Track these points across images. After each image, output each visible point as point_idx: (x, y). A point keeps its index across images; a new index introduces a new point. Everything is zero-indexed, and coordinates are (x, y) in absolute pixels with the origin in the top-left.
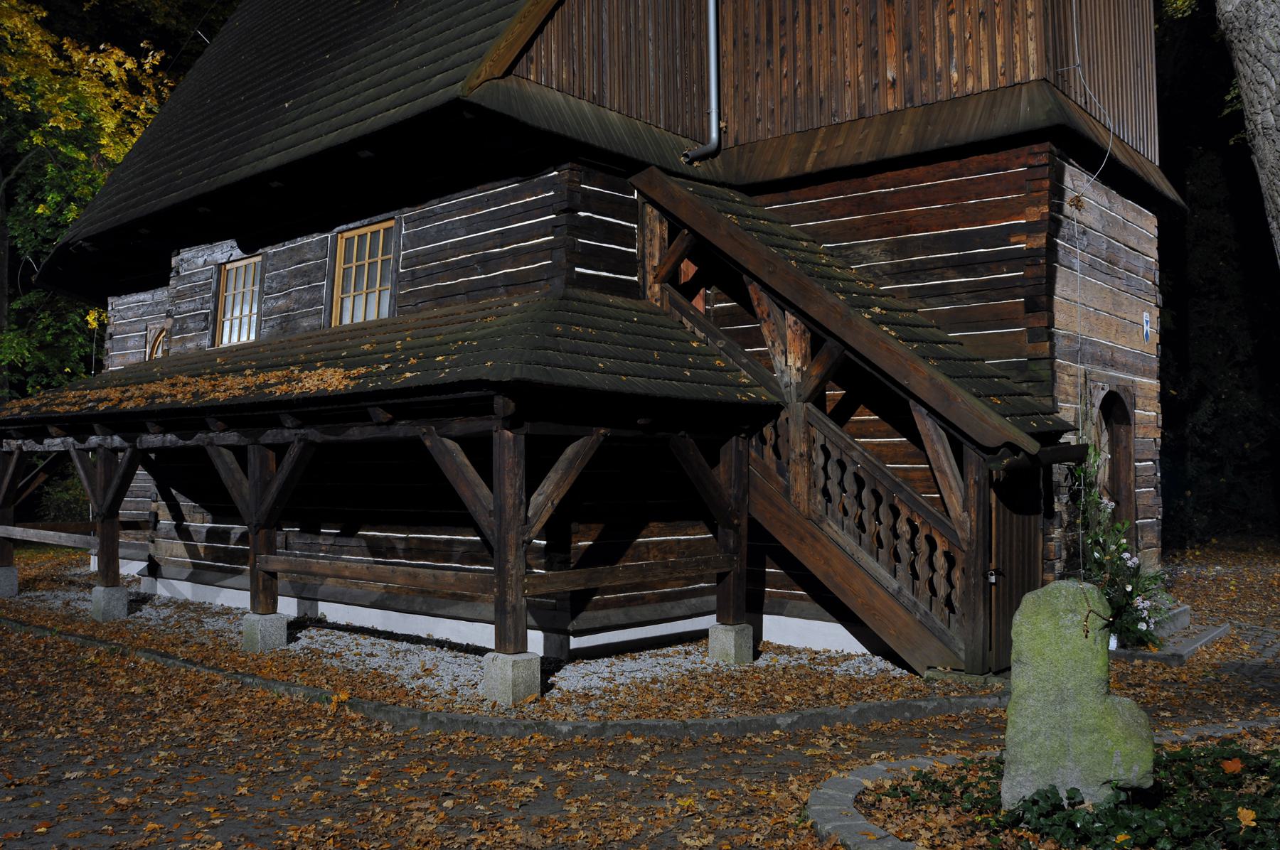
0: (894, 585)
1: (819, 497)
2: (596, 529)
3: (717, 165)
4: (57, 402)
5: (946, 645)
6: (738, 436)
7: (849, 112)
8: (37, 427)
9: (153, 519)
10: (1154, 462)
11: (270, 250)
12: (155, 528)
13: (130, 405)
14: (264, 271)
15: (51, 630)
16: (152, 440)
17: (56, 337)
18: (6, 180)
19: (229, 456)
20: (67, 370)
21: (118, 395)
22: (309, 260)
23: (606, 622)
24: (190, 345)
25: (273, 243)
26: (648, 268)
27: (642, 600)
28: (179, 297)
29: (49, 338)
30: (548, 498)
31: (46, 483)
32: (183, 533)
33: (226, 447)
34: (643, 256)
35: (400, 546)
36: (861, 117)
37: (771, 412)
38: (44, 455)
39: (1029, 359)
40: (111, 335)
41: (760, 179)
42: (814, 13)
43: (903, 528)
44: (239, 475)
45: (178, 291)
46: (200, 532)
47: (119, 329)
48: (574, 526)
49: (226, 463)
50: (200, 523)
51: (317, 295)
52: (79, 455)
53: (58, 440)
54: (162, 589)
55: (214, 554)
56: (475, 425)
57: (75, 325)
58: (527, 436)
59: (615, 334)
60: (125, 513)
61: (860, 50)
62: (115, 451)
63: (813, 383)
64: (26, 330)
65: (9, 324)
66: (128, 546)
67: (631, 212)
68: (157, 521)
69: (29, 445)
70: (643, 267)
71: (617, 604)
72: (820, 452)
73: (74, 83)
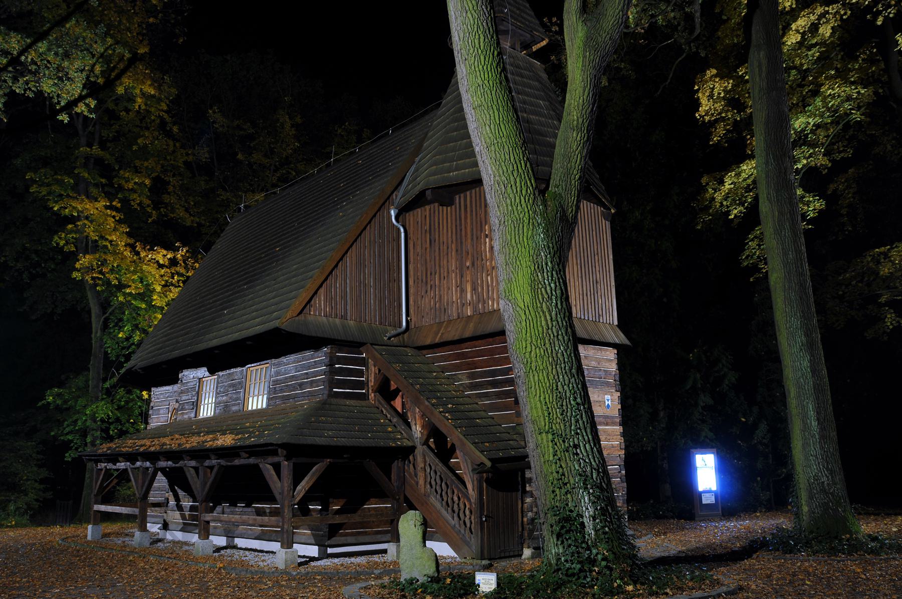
0: (453, 523)
1: (428, 486)
2: (342, 502)
3: (405, 337)
4: (124, 445)
5: (469, 547)
6: (398, 460)
7: (455, 315)
8: (114, 458)
9: (166, 501)
10: (620, 466)
11: (221, 373)
12: (167, 506)
13: (152, 449)
14: (218, 383)
15: (115, 550)
16: (162, 464)
17: (127, 402)
18: (104, 317)
19: (192, 471)
20: (132, 421)
21: (149, 444)
22: (236, 380)
23: (345, 542)
24: (186, 416)
25: (222, 370)
26: (370, 386)
27: (365, 533)
28: (181, 393)
29: (123, 403)
30: (303, 487)
31: (118, 484)
32: (180, 508)
33: (191, 467)
34: (368, 381)
35: (268, 511)
36: (459, 318)
37: (412, 449)
38: (117, 470)
39: (517, 425)
40: (152, 407)
41: (419, 345)
42: (442, 271)
43: (456, 498)
44: (196, 479)
45: (182, 390)
46: (187, 507)
47: (156, 404)
48: (331, 500)
49: (191, 474)
50: (187, 503)
51: (238, 396)
52: (132, 471)
53: (123, 464)
54: (169, 536)
55: (193, 518)
56: (276, 459)
57: (137, 396)
58: (294, 463)
59: (341, 419)
60: (152, 499)
61: (458, 288)
62: (147, 469)
63: (425, 437)
64: (111, 398)
65: (102, 395)
66: (153, 516)
67: (363, 362)
68: (168, 502)
69: (110, 466)
70: (368, 386)
71: (352, 534)
73: (141, 267)
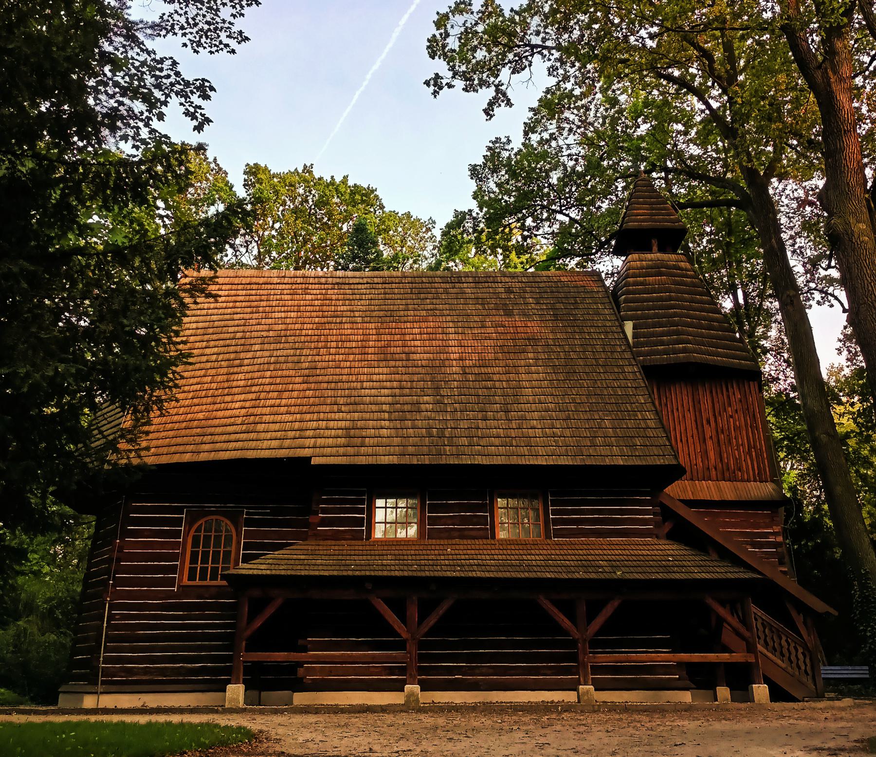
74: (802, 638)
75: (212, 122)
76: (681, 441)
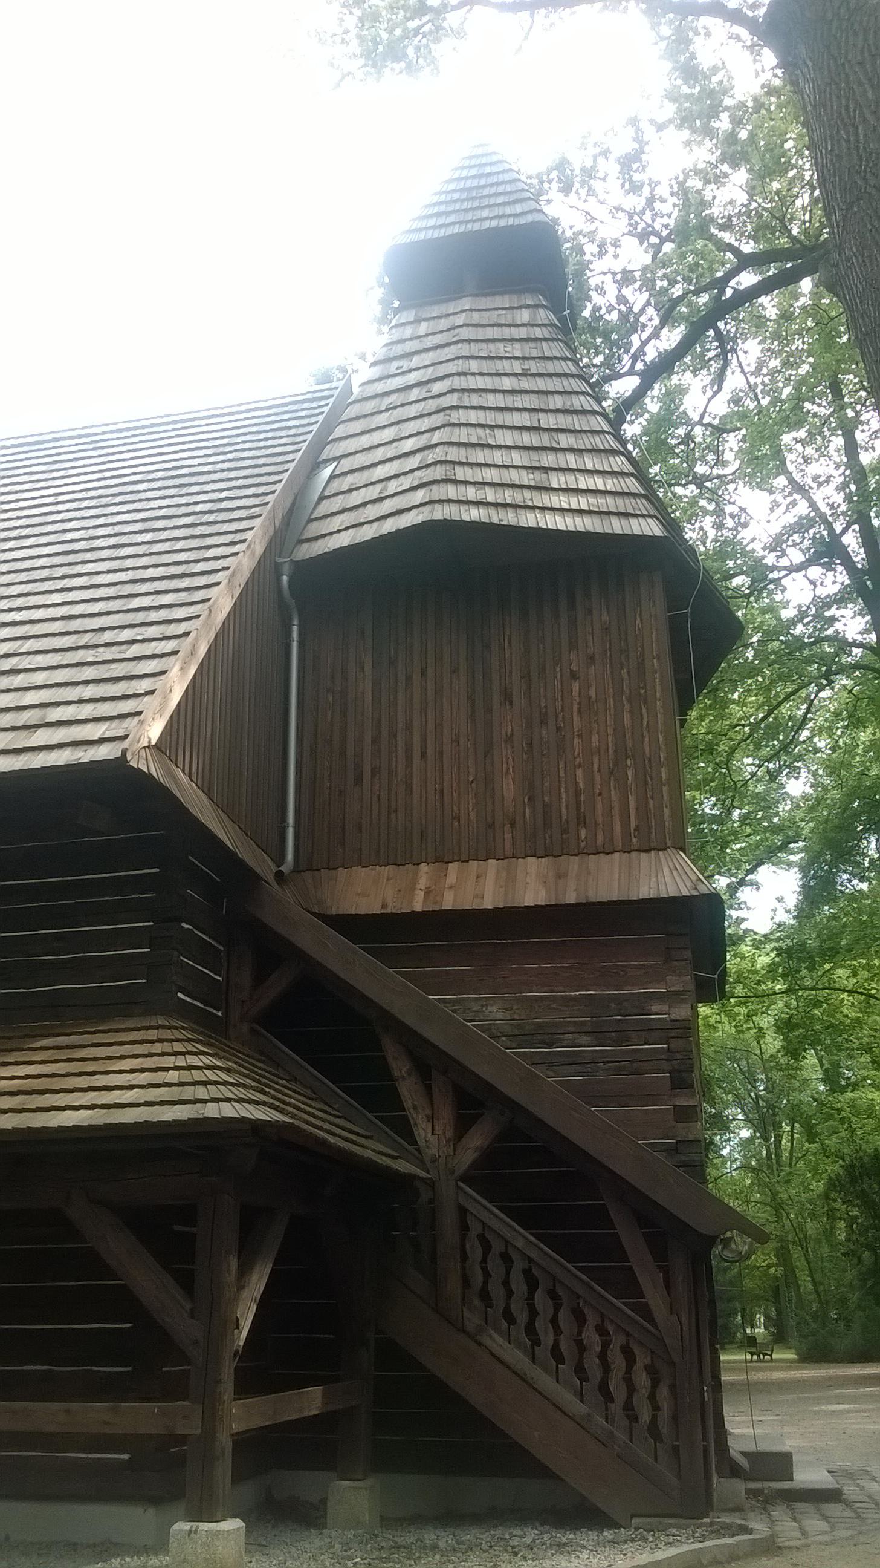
1: (476, 1302)
72: (477, 1243)
74: (651, 1320)
75: (378, 81)
76: (423, 755)
